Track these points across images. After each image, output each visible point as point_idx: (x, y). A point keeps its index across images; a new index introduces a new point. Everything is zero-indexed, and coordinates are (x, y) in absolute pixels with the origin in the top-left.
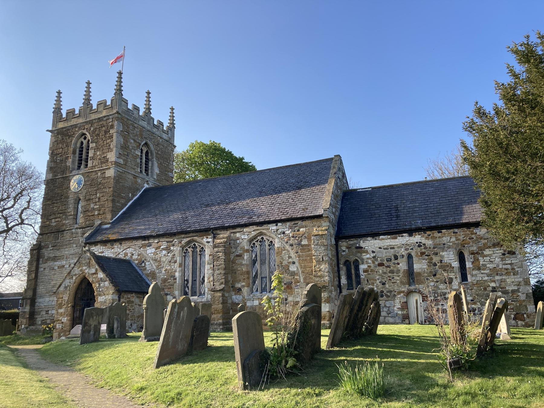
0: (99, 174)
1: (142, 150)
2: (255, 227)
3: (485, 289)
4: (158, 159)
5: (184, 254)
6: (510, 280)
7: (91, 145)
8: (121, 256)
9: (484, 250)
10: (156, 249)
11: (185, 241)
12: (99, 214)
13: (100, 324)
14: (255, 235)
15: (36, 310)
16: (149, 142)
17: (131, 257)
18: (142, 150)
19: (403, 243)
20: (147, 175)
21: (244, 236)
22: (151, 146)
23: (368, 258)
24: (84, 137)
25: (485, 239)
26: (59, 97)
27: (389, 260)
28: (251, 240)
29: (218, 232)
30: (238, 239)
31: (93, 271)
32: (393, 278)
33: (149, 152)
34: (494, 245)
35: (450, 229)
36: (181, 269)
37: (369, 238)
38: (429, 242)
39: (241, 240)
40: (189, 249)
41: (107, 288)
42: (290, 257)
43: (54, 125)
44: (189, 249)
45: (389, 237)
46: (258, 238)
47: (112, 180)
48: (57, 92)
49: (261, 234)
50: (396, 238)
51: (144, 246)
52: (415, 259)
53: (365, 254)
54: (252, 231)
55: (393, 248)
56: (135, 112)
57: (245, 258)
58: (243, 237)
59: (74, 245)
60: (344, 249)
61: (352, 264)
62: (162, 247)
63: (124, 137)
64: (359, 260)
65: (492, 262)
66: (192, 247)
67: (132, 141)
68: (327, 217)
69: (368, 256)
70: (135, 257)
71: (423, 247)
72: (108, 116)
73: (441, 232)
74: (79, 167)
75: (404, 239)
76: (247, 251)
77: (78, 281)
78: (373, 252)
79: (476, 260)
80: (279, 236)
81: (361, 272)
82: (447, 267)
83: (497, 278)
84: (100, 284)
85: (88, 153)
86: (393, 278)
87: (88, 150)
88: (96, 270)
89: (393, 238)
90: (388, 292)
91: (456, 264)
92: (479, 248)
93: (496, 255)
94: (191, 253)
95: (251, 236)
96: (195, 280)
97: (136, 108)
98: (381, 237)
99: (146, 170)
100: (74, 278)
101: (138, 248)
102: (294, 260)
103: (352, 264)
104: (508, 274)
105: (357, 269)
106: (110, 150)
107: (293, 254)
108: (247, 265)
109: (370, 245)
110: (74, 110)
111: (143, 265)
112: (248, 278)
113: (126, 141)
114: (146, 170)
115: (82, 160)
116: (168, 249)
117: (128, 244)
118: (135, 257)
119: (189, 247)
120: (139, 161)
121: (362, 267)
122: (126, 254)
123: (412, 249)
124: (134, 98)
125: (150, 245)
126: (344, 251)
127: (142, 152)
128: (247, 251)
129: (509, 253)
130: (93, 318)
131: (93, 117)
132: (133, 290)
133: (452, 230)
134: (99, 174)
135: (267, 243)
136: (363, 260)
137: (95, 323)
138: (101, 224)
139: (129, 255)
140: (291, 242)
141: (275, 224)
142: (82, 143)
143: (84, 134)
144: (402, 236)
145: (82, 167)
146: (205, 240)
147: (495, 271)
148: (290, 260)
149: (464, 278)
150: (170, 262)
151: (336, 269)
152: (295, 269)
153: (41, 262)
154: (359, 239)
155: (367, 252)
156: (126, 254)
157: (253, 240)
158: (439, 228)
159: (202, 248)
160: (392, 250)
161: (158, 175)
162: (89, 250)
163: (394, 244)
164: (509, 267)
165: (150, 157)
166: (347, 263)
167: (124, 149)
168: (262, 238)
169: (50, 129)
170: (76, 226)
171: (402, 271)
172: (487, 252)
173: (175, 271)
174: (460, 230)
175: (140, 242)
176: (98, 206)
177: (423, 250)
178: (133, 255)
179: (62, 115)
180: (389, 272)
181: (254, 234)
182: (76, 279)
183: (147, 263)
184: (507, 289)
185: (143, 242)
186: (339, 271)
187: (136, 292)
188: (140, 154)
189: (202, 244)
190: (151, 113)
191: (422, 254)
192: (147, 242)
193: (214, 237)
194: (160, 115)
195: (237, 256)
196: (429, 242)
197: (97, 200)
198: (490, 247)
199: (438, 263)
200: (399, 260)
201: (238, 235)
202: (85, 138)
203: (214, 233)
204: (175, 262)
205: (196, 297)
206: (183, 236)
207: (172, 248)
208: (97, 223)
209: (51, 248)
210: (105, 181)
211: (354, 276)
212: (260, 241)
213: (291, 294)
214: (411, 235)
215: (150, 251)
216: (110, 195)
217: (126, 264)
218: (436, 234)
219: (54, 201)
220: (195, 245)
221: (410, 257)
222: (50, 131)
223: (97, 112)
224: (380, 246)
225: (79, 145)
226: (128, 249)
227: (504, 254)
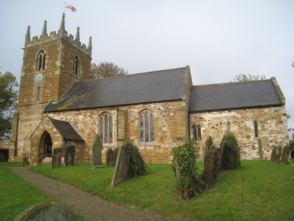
0: (51, 73)
1: (74, 60)
2: (142, 105)
3: (267, 141)
4: (82, 65)
5: (100, 120)
6: (279, 136)
7: (46, 57)
9: (268, 121)
10: (84, 116)
11: (100, 112)
12: (51, 96)
13: (61, 157)
14: (142, 110)
15: (18, 148)
17: (70, 120)
18: (74, 60)
19: (225, 116)
20: (77, 74)
21: (135, 111)
22: (79, 58)
23: (206, 124)
24: (42, 52)
25: (268, 115)
26: (29, 30)
28: (139, 113)
29: (120, 107)
30: (132, 112)
31: (51, 127)
32: (219, 135)
33: (78, 62)
34: (273, 118)
35: (250, 109)
36: (98, 128)
37: (207, 113)
39: (133, 112)
40: (103, 117)
41: (59, 137)
42: (163, 123)
43: (26, 45)
44: (103, 117)
45: (218, 112)
46: (144, 111)
47: (59, 77)
48: (28, 27)
49: (145, 109)
50: (222, 113)
51: (77, 114)
52: (232, 125)
53: (204, 122)
54: (140, 107)
55: (220, 119)
56: (71, 39)
57: (136, 122)
58: (135, 111)
59: (37, 113)
60: (193, 119)
61: (197, 127)
62: (87, 115)
63: (65, 52)
64: (200, 124)
65: (271, 127)
66: (105, 116)
67: (69, 55)
68: (185, 100)
69: (206, 123)
70: (72, 120)
71: (236, 118)
72: (56, 40)
73: (246, 110)
74: (39, 69)
75: (226, 114)
76: (137, 119)
77: (42, 132)
78: (209, 121)
79: (263, 126)
80: (157, 111)
81: (202, 131)
82: (247, 129)
83: (273, 135)
84: (54, 135)
85: (45, 61)
86: (219, 135)
87: (45, 59)
88: (52, 127)
89: (220, 113)
90: (216, 142)
91: (253, 128)
92: (265, 119)
93: (273, 123)
94: (104, 120)
95: (140, 110)
96: (106, 135)
97: (72, 36)
98: (214, 112)
99: (76, 72)
100: (40, 131)
101: (74, 116)
102: (165, 125)
103: (197, 127)
104: (278, 133)
105: (199, 130)
106: (57, 60)
107: (164, 121)
108: (137, 127)
109: (207, 116)
110: (37, 37)
111: (77, 125)
112: (138, 134)
113: (66, 55)
114: (76, 72)
115: (41, 66)
116: (91, 116)
117: (67, 113)
118: (72, 120)
119: (103, 116)
120: (72, 66)
121: (202, 129)
122: (67, 119)
123: (230, 119)
124: (71, 31)
125: (80, 114)
126: (192, 120)
127: (74, 62)
128: (137, 119)
129: (280, 122)
130: (57, 153)
131: (47, 41)
132: (72, 139)
133: (251, 110)
134: (51, 73)
135: (149, 114)
136: (203, 125)
137: (59, 157)
138: (52, 102)
139: (69, 119)
140: (163, 114)
141: (154, 104)
142: (41, 56)
143: (42, 51)
144: (225, 112)
145: (41, 69)
146: (112, 112)
147: (272, 132)
148: (163, 124)
149: (256, 135)
150: (92, 124)
151: (188, 130)
152: (166, 130)
153: (19, 122)
154: (201, 113)
155: (205, 121)
156: (67, 119)
157: (140, 113)
158: (244, 108)
159: (111, 116)
160: (219, 120)
161: (82, 75)
162: (48, 116)
163: (220, 116)
164: (279, 129)
165: (78, 65)
167: (65, 60)
168: (146, 112)
169: (24, 47)
170: (38, 102)
171: (224, 131)
172: (269, 122)
173: (95, 129)
174: (256, 109)
175: (75, 112)
176: (50, 91)
177: (236, 120)
178: (71, 119)
179: (30, 40)
180: (217, 132)
181: (141, 109)
182: (41, 131)
183: (79, 124)
184: (277, 141)
185: (77, 112)
186: (189, 131)
187: (74, 140)
188: (73, 62)
189: (111, 114)
190: (79, 40)
192: (79, 112)
193: (118, 111)
194: (84, 41)
195: (132, 121)
196: (239, 116)
197: (50, 88)
198: (270, 119)
199: (243, 127)
200: (222, 126)
201: (132, 109)
202: (43, 53)
203: (118, 108)
204: (95, 124)
205: (108, 144)
206: (99, 109)
207: (93, 116)
208: (50, 101)
209: (25, 115)
210: (54, 77)
211: (197, 134)
212: (145, 113)
213: (163, 143)
214: (229, 112)
215: (81, 117)
216: (57, 85)
217: (67, 124)
218: (243, 111)
219: (26, 88)
220: (106, 114)
222: (24, 49)
223: (50, 37)
224: (212, 117)
225: (39, 57)
226: (68, 116)
227: (277, 123)
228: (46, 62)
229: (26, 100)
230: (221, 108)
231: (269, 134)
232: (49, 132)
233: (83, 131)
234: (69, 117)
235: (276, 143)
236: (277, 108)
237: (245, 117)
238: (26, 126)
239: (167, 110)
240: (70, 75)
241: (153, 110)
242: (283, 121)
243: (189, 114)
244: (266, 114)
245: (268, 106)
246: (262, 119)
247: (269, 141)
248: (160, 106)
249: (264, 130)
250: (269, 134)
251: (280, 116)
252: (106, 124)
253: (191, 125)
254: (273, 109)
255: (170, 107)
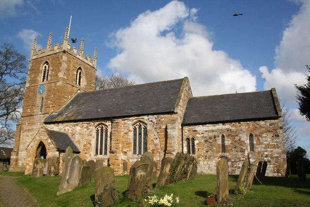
2: (136, 118)
4: (86, 76)
8: (62, 131)
10: (81, 127)
16: (82, 67)
27: (210, 138)
34: (269, 131)
37: (201, 126)
38: (233, 128)
52: (226, 138)
67: (72, 66)
70: (70, 131)
75: (220, 126)
78: (202, 133)
79: (258, 140)
81: (195, 144)
91: (248, 142)
99: (79, 83)
111: (74, 136)
114: (79, 83)
116: (87, 128)
117: (66, 124)
118: (70, 131)
121: (196, 142)
127: (77, 73)
129: (276, 136)
139: (67, 130)
142: (45, 67)
147: (268, 146)
151: (181, 143)
158: (239, 121)
164: (275, 143)
166: (188, 139)
172: (264, 135)
175: (72, 123)
181: (135, 121)
191: (229, 135)
192: (76, 123)
195: (125, 133)
207: (90, 127)
210: (55, 89)
215: (78, 128)
221: (223, 136)
228: (49, 74)
229: (29, 111)
230: (215, 120)
231: (265, 148)
232: (45, 143)
233: (79, 142)
234: (67, 128)
235: (271, 158)
236: (273, 121)
237: (239, 130)
238: (27, 136)
239: (159, 122)
240: (73, 86)
241: (146, 122)
242: (280, 135)
243: (182, 127)
244: (261, 127)
245: (263, 119)
246: (257, 133)
247: (264, 155)
248: (153, 118)
249: (260, 143)
250: (265, 148)
251: (276, 130)
252: (102, 135)
253: (185, 138)
254: (269, 122)
255: (162, 120)
